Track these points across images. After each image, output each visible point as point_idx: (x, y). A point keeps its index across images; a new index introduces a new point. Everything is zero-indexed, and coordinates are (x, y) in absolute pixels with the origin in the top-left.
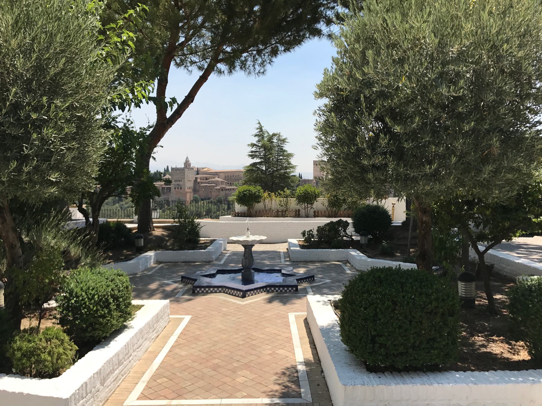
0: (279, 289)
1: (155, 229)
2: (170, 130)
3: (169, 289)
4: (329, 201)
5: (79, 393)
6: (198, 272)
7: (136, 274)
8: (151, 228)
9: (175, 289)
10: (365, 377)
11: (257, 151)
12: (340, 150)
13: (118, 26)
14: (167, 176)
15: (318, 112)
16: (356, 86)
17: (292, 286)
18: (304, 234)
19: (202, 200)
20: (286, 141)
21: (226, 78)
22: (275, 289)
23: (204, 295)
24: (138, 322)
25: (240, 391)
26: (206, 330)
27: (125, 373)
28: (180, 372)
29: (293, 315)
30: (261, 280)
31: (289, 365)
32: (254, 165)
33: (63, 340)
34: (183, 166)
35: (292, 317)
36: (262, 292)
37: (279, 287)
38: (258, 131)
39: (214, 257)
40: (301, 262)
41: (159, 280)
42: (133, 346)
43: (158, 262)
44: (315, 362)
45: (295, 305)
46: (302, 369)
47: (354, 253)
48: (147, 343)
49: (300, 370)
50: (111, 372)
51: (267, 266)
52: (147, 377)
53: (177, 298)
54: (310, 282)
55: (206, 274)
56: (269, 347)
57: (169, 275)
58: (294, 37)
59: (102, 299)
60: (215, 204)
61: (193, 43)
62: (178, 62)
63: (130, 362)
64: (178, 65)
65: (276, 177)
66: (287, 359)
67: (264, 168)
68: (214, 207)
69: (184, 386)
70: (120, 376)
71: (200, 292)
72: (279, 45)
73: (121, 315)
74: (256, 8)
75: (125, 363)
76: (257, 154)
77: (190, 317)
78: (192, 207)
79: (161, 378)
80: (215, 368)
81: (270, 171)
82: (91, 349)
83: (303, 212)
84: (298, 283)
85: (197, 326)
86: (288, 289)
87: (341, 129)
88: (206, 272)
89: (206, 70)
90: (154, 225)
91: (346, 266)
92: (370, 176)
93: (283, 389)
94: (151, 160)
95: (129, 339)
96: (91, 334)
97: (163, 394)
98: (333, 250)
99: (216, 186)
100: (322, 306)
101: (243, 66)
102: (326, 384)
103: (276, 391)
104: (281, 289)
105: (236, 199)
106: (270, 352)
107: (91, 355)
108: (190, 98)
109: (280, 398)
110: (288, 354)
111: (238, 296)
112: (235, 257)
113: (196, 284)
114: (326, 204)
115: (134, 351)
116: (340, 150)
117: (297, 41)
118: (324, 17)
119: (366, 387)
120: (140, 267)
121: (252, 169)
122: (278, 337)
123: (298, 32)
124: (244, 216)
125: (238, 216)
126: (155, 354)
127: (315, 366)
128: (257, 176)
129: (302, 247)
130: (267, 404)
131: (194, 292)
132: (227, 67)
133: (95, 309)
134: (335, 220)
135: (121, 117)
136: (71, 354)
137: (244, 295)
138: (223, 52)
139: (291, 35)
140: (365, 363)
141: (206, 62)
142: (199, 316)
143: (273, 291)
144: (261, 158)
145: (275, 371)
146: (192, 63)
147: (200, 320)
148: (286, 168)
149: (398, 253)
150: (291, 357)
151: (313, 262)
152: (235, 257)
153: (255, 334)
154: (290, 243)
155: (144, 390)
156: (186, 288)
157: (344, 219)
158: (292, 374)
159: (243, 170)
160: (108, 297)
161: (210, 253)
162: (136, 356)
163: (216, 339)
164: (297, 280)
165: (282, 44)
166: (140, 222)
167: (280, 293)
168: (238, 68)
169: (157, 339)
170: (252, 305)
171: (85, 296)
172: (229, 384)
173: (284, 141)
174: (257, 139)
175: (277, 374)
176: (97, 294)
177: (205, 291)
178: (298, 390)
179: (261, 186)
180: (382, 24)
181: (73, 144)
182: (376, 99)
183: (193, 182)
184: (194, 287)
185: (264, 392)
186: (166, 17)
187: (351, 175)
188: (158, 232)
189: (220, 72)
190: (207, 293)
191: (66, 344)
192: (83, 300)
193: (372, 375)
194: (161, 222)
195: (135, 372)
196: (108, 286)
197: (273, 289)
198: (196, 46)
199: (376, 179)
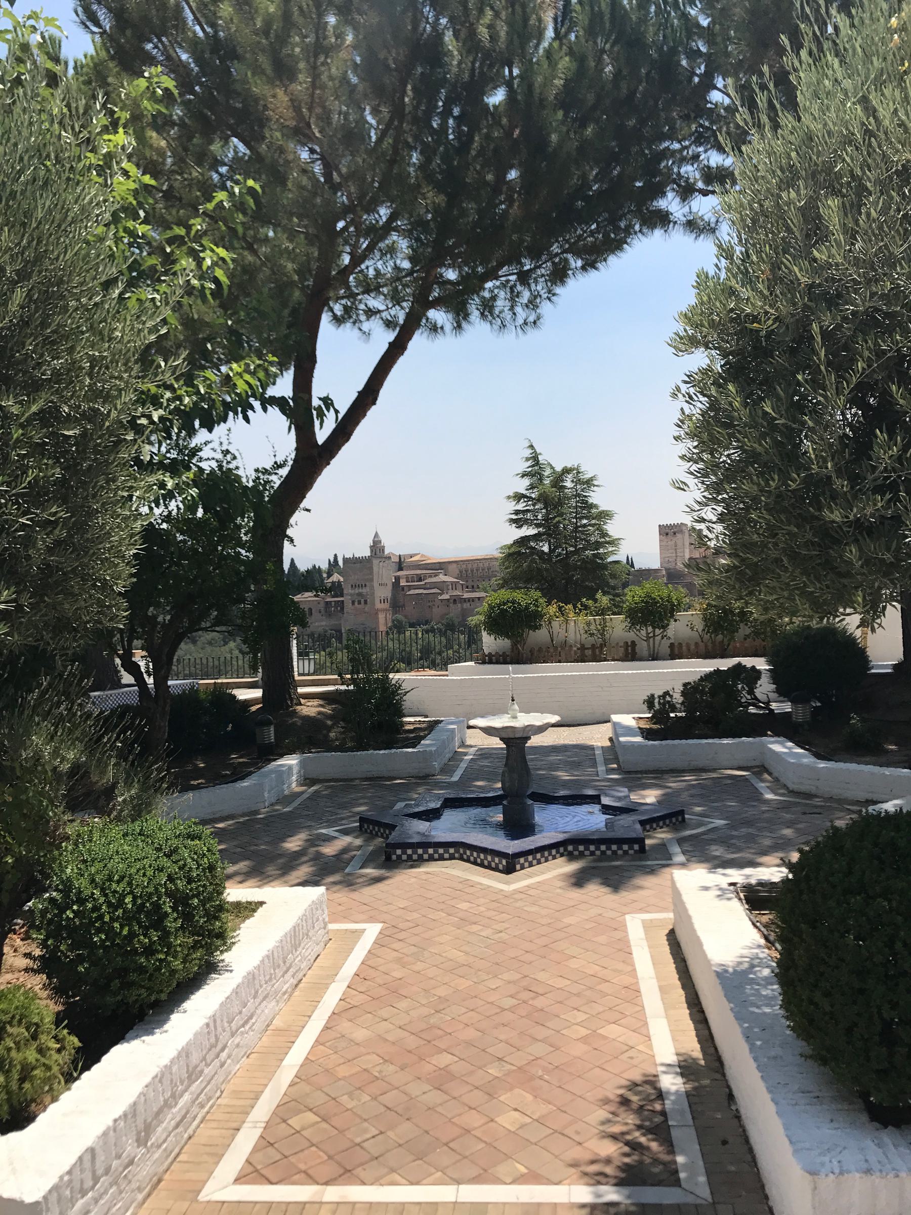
0: (598, 849)
1: (303, 701)
2: (327, 472)
3: (329, 850)
4: (705, 619)
5: (70, 1181)
6: (400, 805)
7: (257, 812)
8: (292, 699)
9: (345, 851)
10: (869, 1143)
11: (528, 511)
12: (759, 485)
13: (193, 233)
14: (336, 577)
15: (684, 388)
16: (794, 304)
17: (631, 841)
18: (650, 702)
19: (412, 625)
20: (595, 483)
21: (447, 342)
22: (587, 849)
23: (412, 867)
24: (248, 949)
25: (508, 1157)
26: (419, 966)
27: (209, 1099)
28: (350, 1095)
29: (635, 921)
30: (554, 822)
31: (637, 1077)
32: (523, 541)
33: (36, 1024)
34: (367, 553)
35: (635, 925)
36: (554, 858)
37: (599, 842)
38: (529, 463)
39: (436, 765)
40: (646, 772)
41: (309, 827)
42: (230, 1022)
43: (308, 780)
44: (707, 1066)
45: (641, 893)
46: (673, 1088)
47: (780, 747)
48: (269, 1007)
49: (668, 1093)
50: (167, 1105)
51: (565, 784)
52: (262, 1111)
53: (349, 874)
54: (675, 828)
55: (417, 810)
56: (581, 1017)
57: (333, 813)
58: (606, 235)
59: (143, 905)
60: (442, 633)
61: (370, 267)
62: (339, 313)
63: (222, 1065)
64: (338, 321)
65: (575, 568)
66: (631, 1053)
67: (546, 549)
68: (436, 641)
69: (358, 1140)
70: (195, 1109)
71: (404, 857)
72: (569, 256)
73: (196, 942)
74: (513, 175)
75: (206, 1071)
76: (529, 516)
77: (378, 927)
78: (391, 644)
79: (300, 1112)
80: (442, 1080)
81: (560, 554)
82: (119, 1037)
83: (643, 648)
84: (644, 830)
85: (395, 954)
86: (620, 848)
87: (754, 425)
88: (417, 805)
89: (403, 327)
90: (300, 690)
91: (763, 781)
92: (852, 553)
93: (626, 1155)
94: (286, 543)
95: (216, 1006)
96: (119, 998)
97: (302, 1167)
98: (725, 741)
99: (441, 594)
100: (717, 902)
101: (487, 309)
102: (747, 1141)
103: (608, 1161)
104: (603, 848)
105: (485, 623)
106: (583, 1032)
107: (118, 1055)
108: (368, 396)
109: (620, 1183)
110: (633, 1039)
111: (496, 869)
112: (486, 763)
113: (394, 837)
114: (699, 625)
115: (233, 1035)
116: (759, 485)
117: (611, 244)
118: (674, 181)
119: (876, 1179)
120: (266, 795)
121: (519, 552)
122: (604, 987)
123: (613, 221)
124: (505, 662)
125: (490, 662)
126: (289, 1036)
127: (707, 1073)
128: (529, 566)
129: (647, 734)
130: (583, 1206)
131: (388, 858)
132: (450, 316)
133: (125, 932)
134: (725, 664)
135: (210, 446)
136: (58, 1060)
137: (510, 864)
138: (438, 283)
139: (597, 231)
140: (864, 1096)
141: (402, 308)
142: (401, 926)
143: (581, 855)
144: (538, 526)
145: (600, 1094)
146: (371, 313)
147: (402, 936)
148: (598, 545)
149: (891, 744)
150: (641, 1048)
151: (677, 772)
152: (486, 763)
153: (542, 976)
154: (616, 725)
155: (255, 1150)
156: (371, 848)
157: (748, 662)
158: (642, 1100)
159: (497, 554)
160: (159, 899)
161: (426, 756)
162: (238, 1046)
163: (442, 992)
164: (643, 823)
165: (577, 254)
166: (266, 685)
167: (599, 860)
168: (475, 315)
169: (296, 993)
170: (531, 892)
171: (102, 900)
172: (477, 1133)
173: (589, 483)
174: (526, 482)
175: (606, 1101)
176: (131, 892)
177: (415, 857)
178: (666, 1158)
179: (541, 590)
180: (863, 124)
181: (53, 510)
182: (853, 339)
183: (390, 587)
184: (388, 845)
185: (574, 1165)
186: (304, 209)
187: (794, 556)
188: (309, 709)
189: (435, 329)
190: (421, 861)
191: (43, 1038)
192: (96, 909)
193: (888, 1136)
194: (314, 685)
195: (236, 1094)
196: (161, 870)
197: (581, 848)
198: (378, 273)
199: (867, 562)
